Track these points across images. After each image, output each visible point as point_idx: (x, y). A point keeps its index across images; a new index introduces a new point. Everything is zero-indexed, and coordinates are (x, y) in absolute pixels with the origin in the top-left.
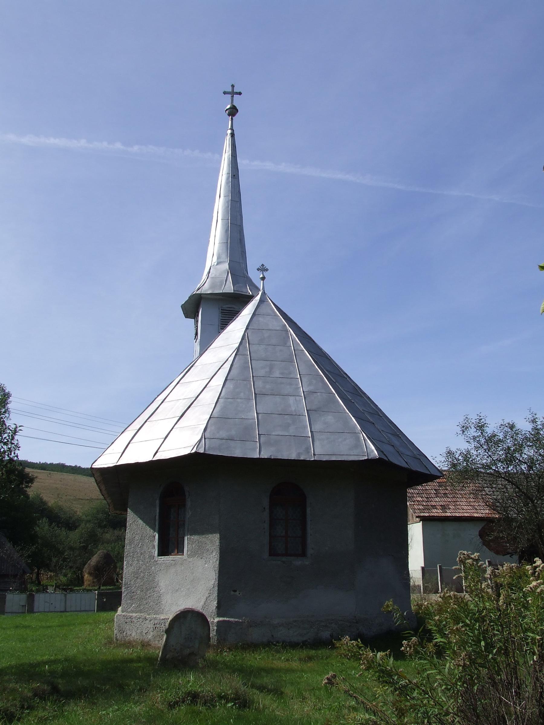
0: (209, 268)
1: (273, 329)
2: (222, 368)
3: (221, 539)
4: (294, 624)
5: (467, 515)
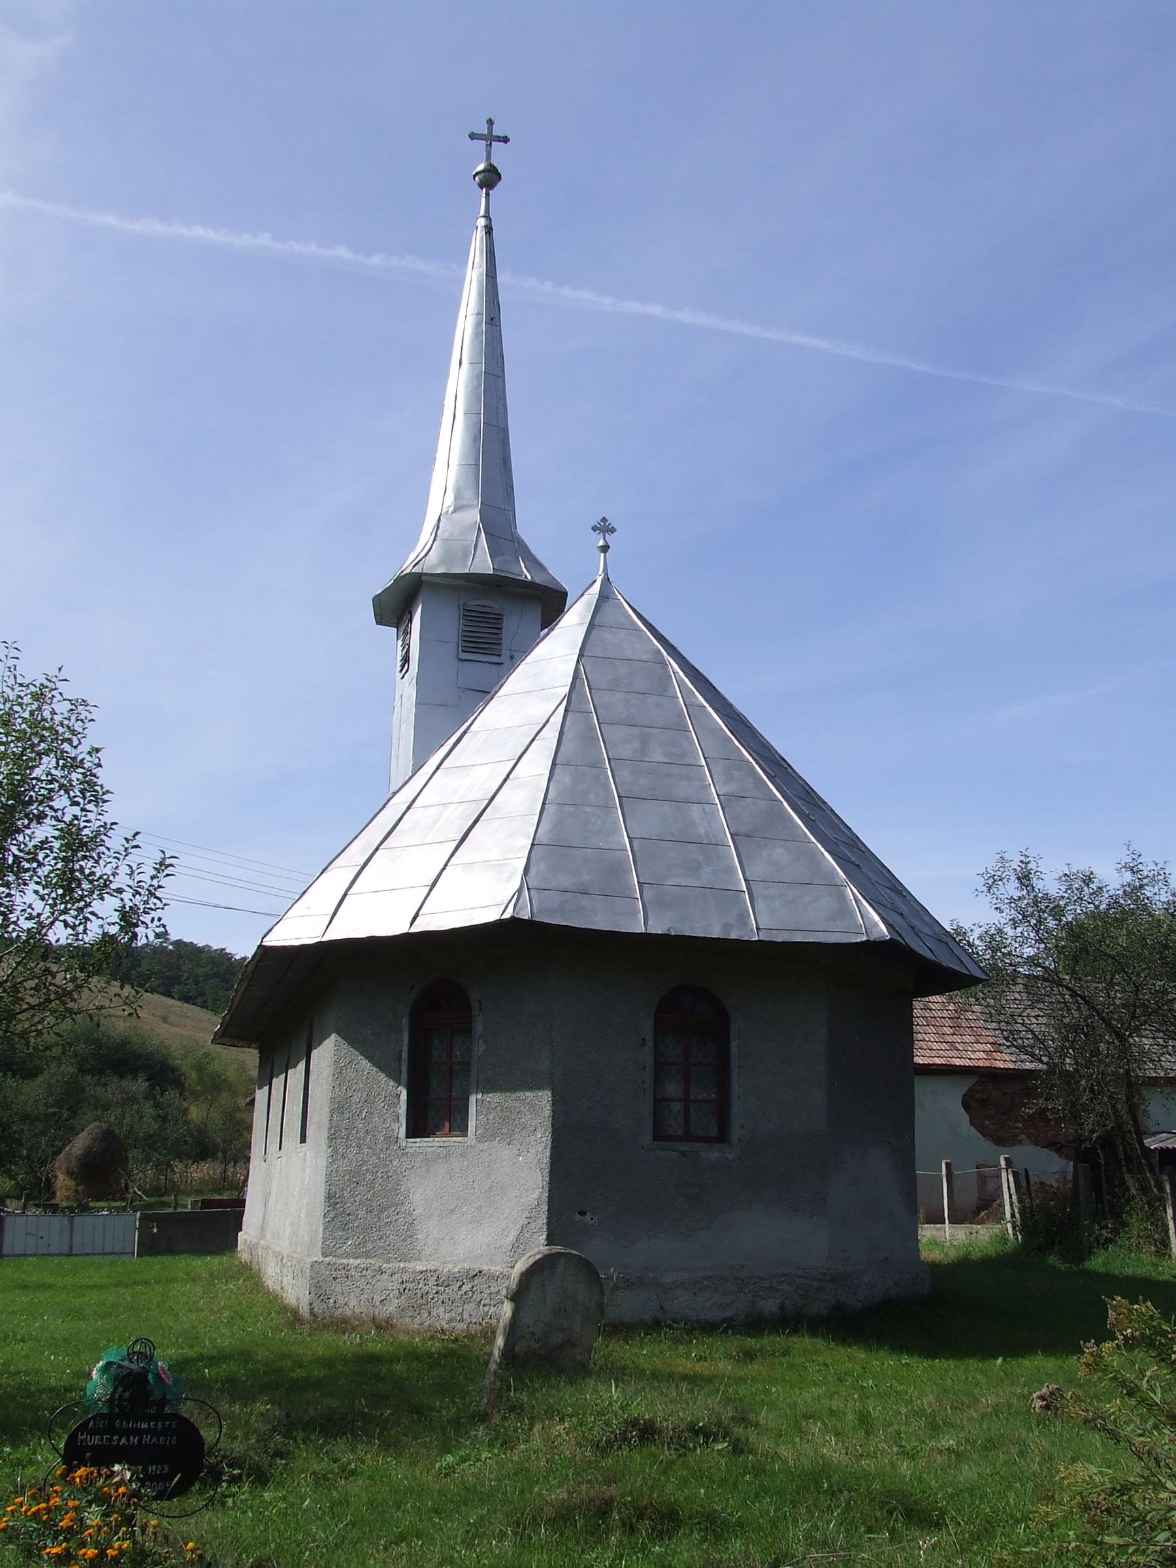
0: (437, 518)
1: (633, 658)
2: (537, 738)
3: (555, 1103)
5: (939, 1063)
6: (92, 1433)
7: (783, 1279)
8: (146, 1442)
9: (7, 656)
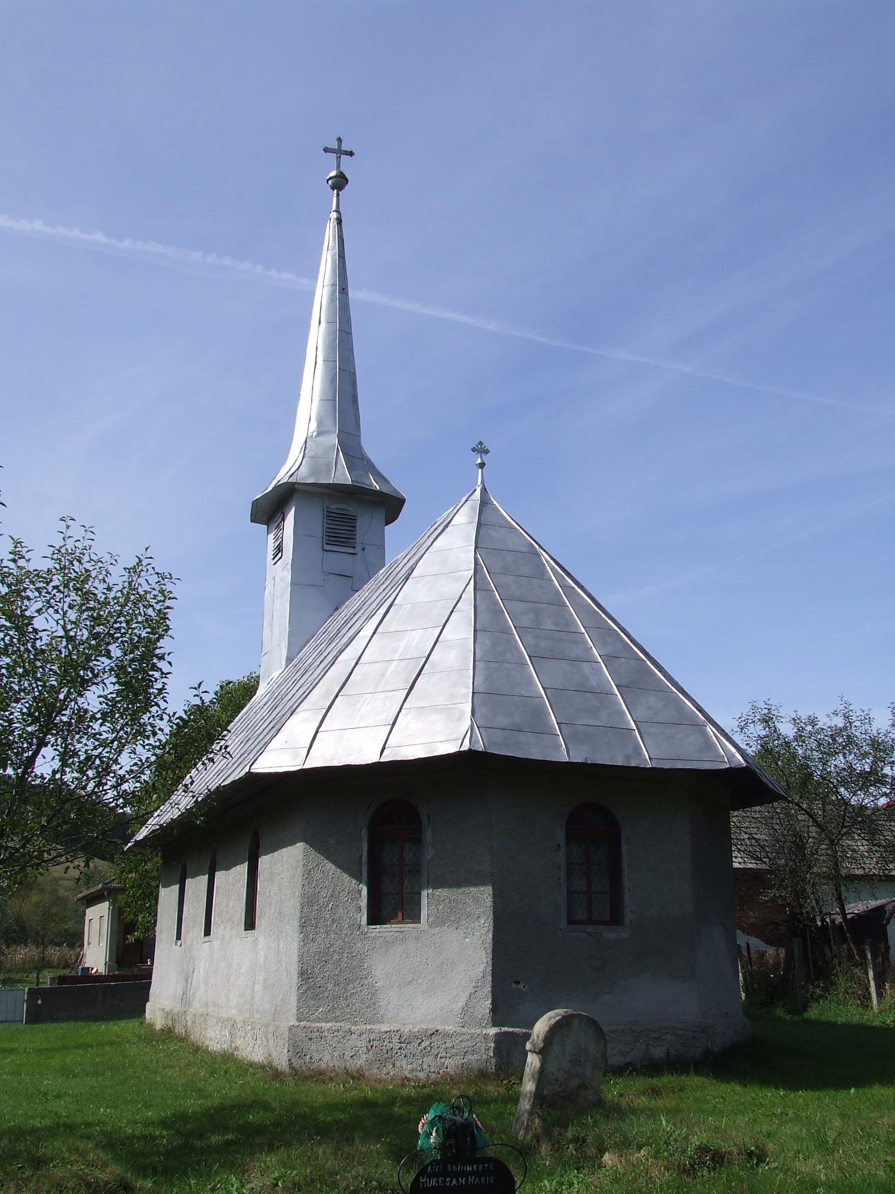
0: (305, 440)
1: (515, 550)
3: (495, 896)
4: (611, 1035)
6: (430, 1176)
7: (667, 1031)
8: (471, 1182)
9: (83, 537)
